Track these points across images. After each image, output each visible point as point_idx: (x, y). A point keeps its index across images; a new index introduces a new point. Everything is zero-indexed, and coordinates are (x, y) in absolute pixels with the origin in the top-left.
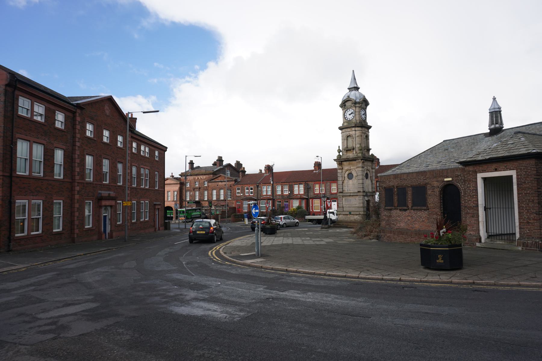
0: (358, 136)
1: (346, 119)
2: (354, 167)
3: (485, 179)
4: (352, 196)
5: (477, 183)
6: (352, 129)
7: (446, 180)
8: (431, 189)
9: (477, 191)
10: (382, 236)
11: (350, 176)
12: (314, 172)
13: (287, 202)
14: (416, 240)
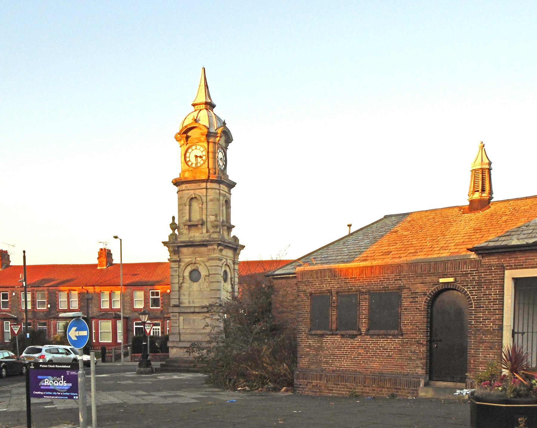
0: (212, 200)
1: (188, 165)
2: (202, 259)
3: (516, 281)
4: (198, 313)
5: (503, 287)
6: (200, 186)
7: (442, 280)
8: (409, 298)
9: (503, 302)
10: (301, 385)
11: (195, 276)
12: (98, 268)
13: (44, 324)
14: (374, 390)
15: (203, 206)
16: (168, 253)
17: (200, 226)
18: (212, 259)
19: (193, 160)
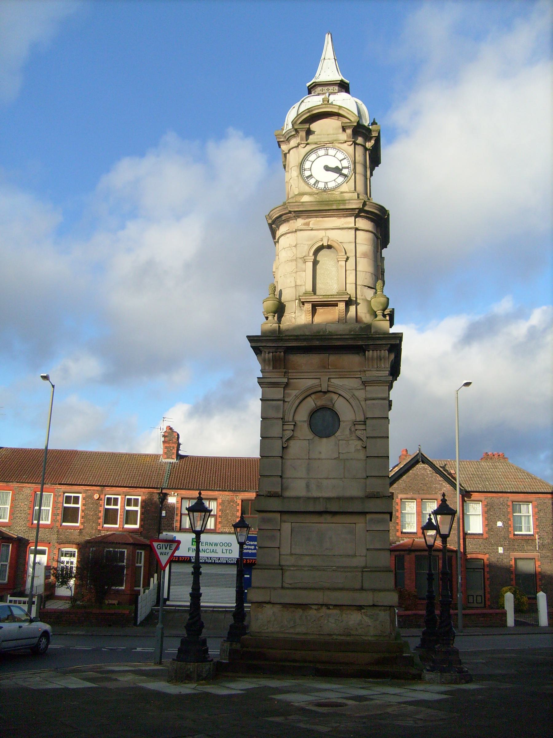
1: (308, 184)
6: (308, 224)
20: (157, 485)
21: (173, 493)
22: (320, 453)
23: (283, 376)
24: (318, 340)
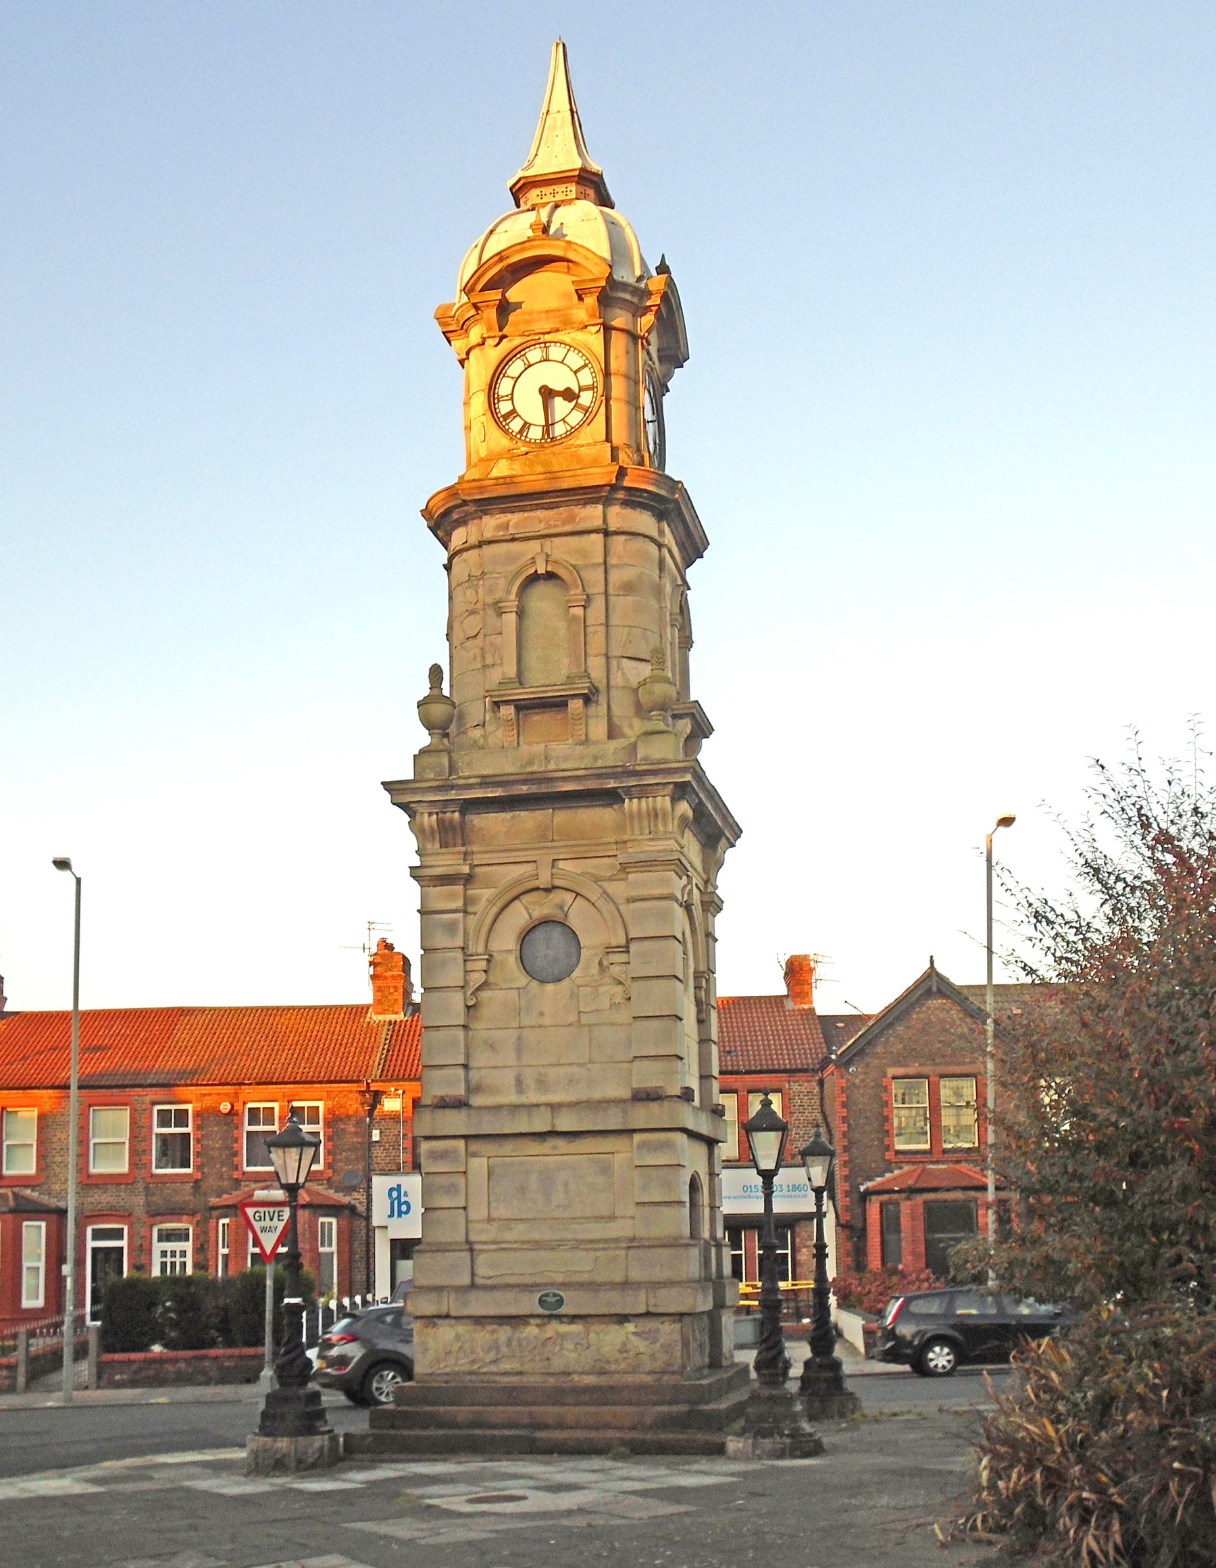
0: (629, 588)
1: (506, 432)
15: (589, 611)
16: (412, 842)
17: (576, 705)
18: (647, 864)
19: (530, 408)
20: (359, 1076)
21: (393, 1089)
22: (542, 1014)
23: (462, 862)
24: (525, 782)
